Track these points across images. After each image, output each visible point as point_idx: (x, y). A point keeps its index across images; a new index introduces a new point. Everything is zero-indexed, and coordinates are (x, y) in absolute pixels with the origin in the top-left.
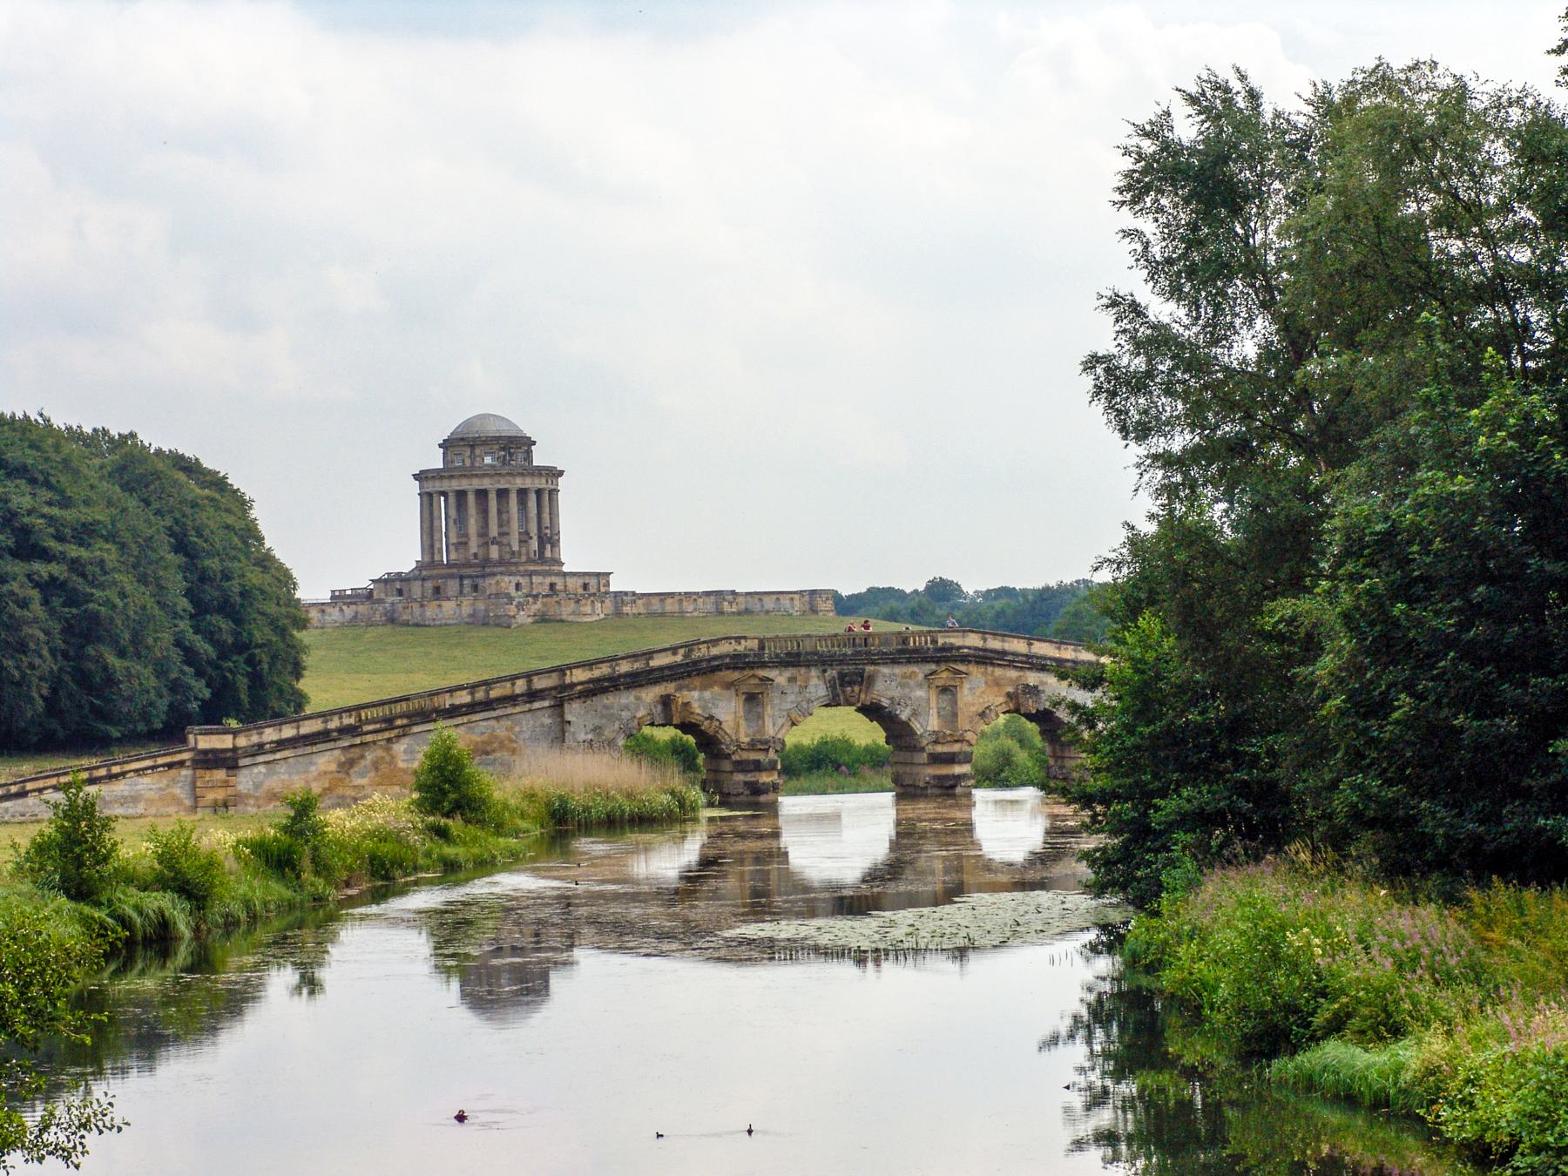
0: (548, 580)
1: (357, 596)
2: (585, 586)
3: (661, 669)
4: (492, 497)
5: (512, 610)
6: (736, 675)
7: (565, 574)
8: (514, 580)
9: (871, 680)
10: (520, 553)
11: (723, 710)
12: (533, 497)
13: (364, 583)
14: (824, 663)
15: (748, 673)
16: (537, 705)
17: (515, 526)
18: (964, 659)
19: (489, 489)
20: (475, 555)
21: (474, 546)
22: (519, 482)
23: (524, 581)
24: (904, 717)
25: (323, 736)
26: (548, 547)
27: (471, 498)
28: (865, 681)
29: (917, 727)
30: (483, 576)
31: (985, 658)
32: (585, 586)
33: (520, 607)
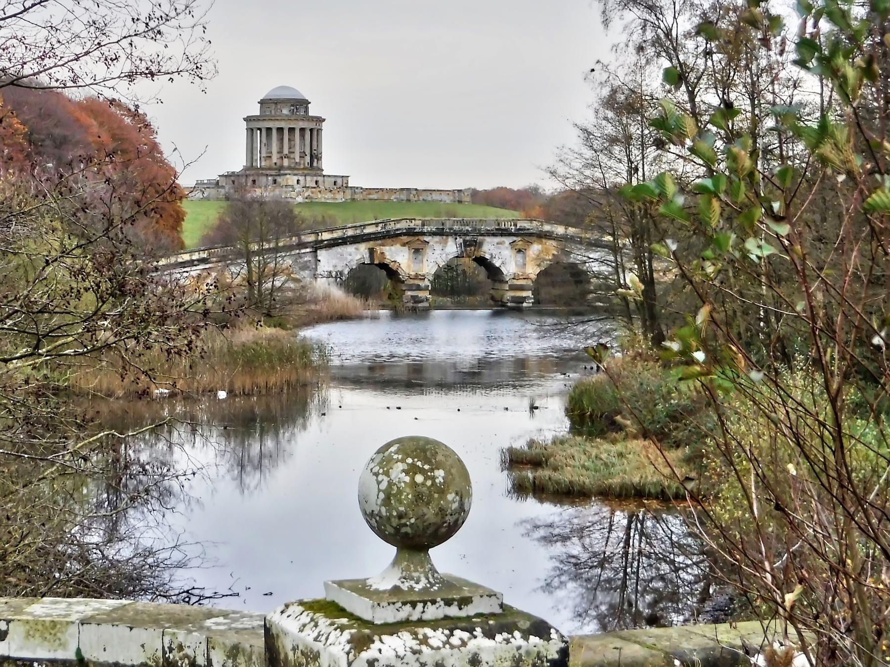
0: (315, 178)
1: (210, 184)
2: (335, 183)
4: (286, 132)
5: (293, 194)
8: (296, 178)
9: (481, 244)
10: (300, 164)
11: (398, 256)
14: (456, 234)
16: (303, 251)
17: (297, 149)
19: (286, 124)
21: (275, 158)
23: (301, 178)
24: (497, 265)
27: (274, 132)
28: (478, 245)
29: (503, 269)
32: (335, 183)
33: (299, 194)
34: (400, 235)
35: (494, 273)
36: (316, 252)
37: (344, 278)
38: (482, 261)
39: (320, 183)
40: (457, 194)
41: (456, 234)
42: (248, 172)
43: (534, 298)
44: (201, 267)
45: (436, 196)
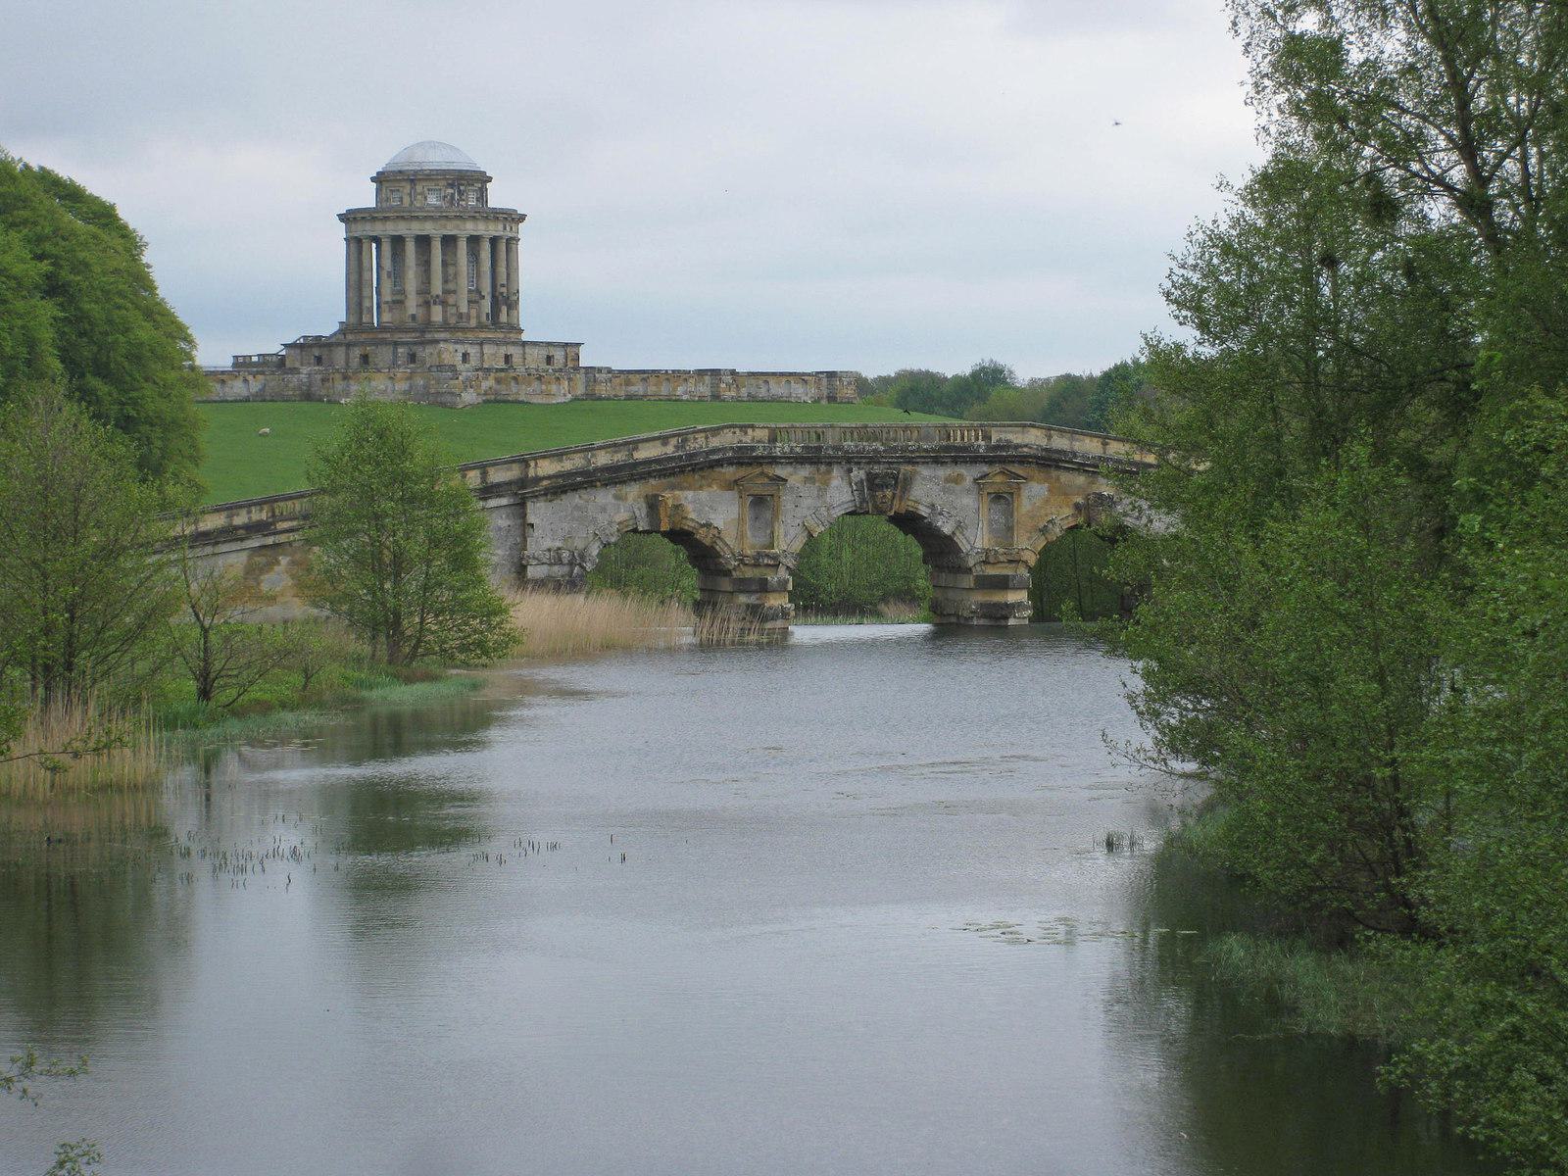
0: (503, 350)
2: (549, 359)
3: (648, 462)
6: (742, 472)
7: (524, 344)
8: (461, 349)
10: (469, 317)
11: (714, 510)
12: (486, 246)
13: (274, 347)
14: (849, 461)
15: (758, 470)
16: (492, 503)
17: (464, 284)
18: (1023, 460)
19: (432, 238)
20: (413, 317)
21: (412, 305)
22: (470, 228)
23: (473, 350)
24: (947, 530)
25: (229, 534)
26: (504, 309)
27: (410, 248)
28: (904, 484)
30: (423, 343)
31: (1049, 461)
32: (549, 359)
33: (468, 384)
34: (719, 463)
35: (940, 550)
36: (522, 505)
37: (589, 566)
38: (909, 522)
39: (516, 360)
40: (825, 381)
41: (849, 460)
42: (350, 337)
43: (1034, 608)
44: (254, 543)
45: (777, 389)
